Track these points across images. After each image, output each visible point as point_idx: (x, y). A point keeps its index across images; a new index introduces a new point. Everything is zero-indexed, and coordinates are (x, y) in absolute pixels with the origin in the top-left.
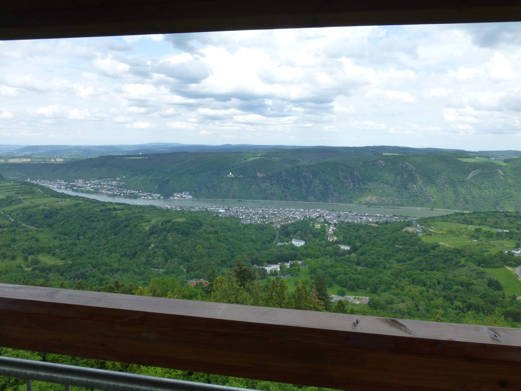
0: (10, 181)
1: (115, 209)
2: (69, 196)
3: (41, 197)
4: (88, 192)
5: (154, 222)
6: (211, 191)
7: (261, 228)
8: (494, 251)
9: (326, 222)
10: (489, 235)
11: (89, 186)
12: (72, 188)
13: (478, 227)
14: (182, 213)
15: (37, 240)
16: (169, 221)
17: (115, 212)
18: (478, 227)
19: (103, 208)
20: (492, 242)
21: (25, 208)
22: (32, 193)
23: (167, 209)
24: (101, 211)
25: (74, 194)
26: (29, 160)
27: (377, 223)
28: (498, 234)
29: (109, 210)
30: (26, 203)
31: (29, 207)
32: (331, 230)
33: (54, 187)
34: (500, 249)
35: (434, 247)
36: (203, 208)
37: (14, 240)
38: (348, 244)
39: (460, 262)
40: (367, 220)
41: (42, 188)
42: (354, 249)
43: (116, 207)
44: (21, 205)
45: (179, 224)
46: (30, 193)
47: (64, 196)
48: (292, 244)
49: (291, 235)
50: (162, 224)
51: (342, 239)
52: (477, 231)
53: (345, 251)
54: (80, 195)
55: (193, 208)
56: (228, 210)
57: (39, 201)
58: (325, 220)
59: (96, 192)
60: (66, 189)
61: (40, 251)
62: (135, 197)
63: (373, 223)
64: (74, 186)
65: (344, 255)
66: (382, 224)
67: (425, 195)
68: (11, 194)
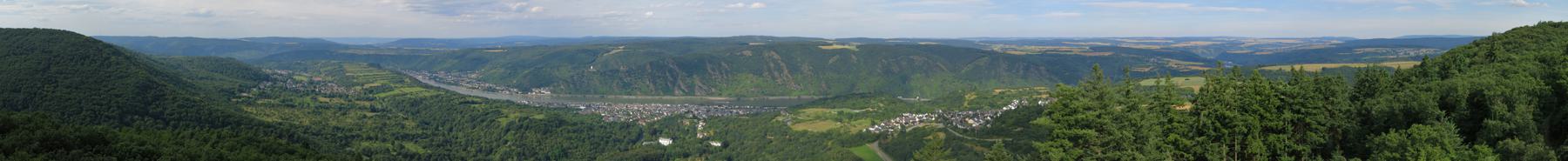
0: (385, 71)
1: (473, 103)
2: (432, 87)
3: (410, 86)
4: (450, 84)
5: (512, 116)
6: (571, 86)
7: (626, 126)
8: (854, 131)
9: (694, 117)
10: (851, 117)
11: (450, 78)
12: (435, 79)
13: (840, 110)
14: (540, 109)
15: (403, 127)
16: (527, 118)
17: (473, 105)
18: (840, 110)
19: (462, 100)
20: (853, 123)
21: (395, 96)
22: (402, 82)
23: (525, 105)
24: (461, 103)
25: (437, 85)
26: (1158, 47)
27: (747, 115)
28: (857, 114)
29: (468, 102)
30: (396, 92)
31: (398, 95)
32: (700, 126)
33: (420, 78)
34: (859, 128)
35: (804, 133)
36: (563, 104)
37: (385, 124)
38: (719, 140)
39: (827, 146)
40: (737, 113)
41: (411, 78)
42: (725, 145)
43: (475, 100)
44: (392, 93)
45: (536, 121)
46: (401, 82)
47: (427, 86)
48: (659, 143)
49: (658, 134)
50: (519, 121)
51: (712, 134)
52: (840, 113)
53: (716, 147)
54: (442, 86)
55: (553, 104)
56: (589, 107)
57: (407, 90)
58: (694, 116)
59: (456, 84)
60: (430, 79)
61: (406, 137)
62: (493, 91)
63: (744, 115)
64: (437, 77)
65: (717, 152)
66: (753, 115)
67: (1172, 137)
68: (385, 82)
